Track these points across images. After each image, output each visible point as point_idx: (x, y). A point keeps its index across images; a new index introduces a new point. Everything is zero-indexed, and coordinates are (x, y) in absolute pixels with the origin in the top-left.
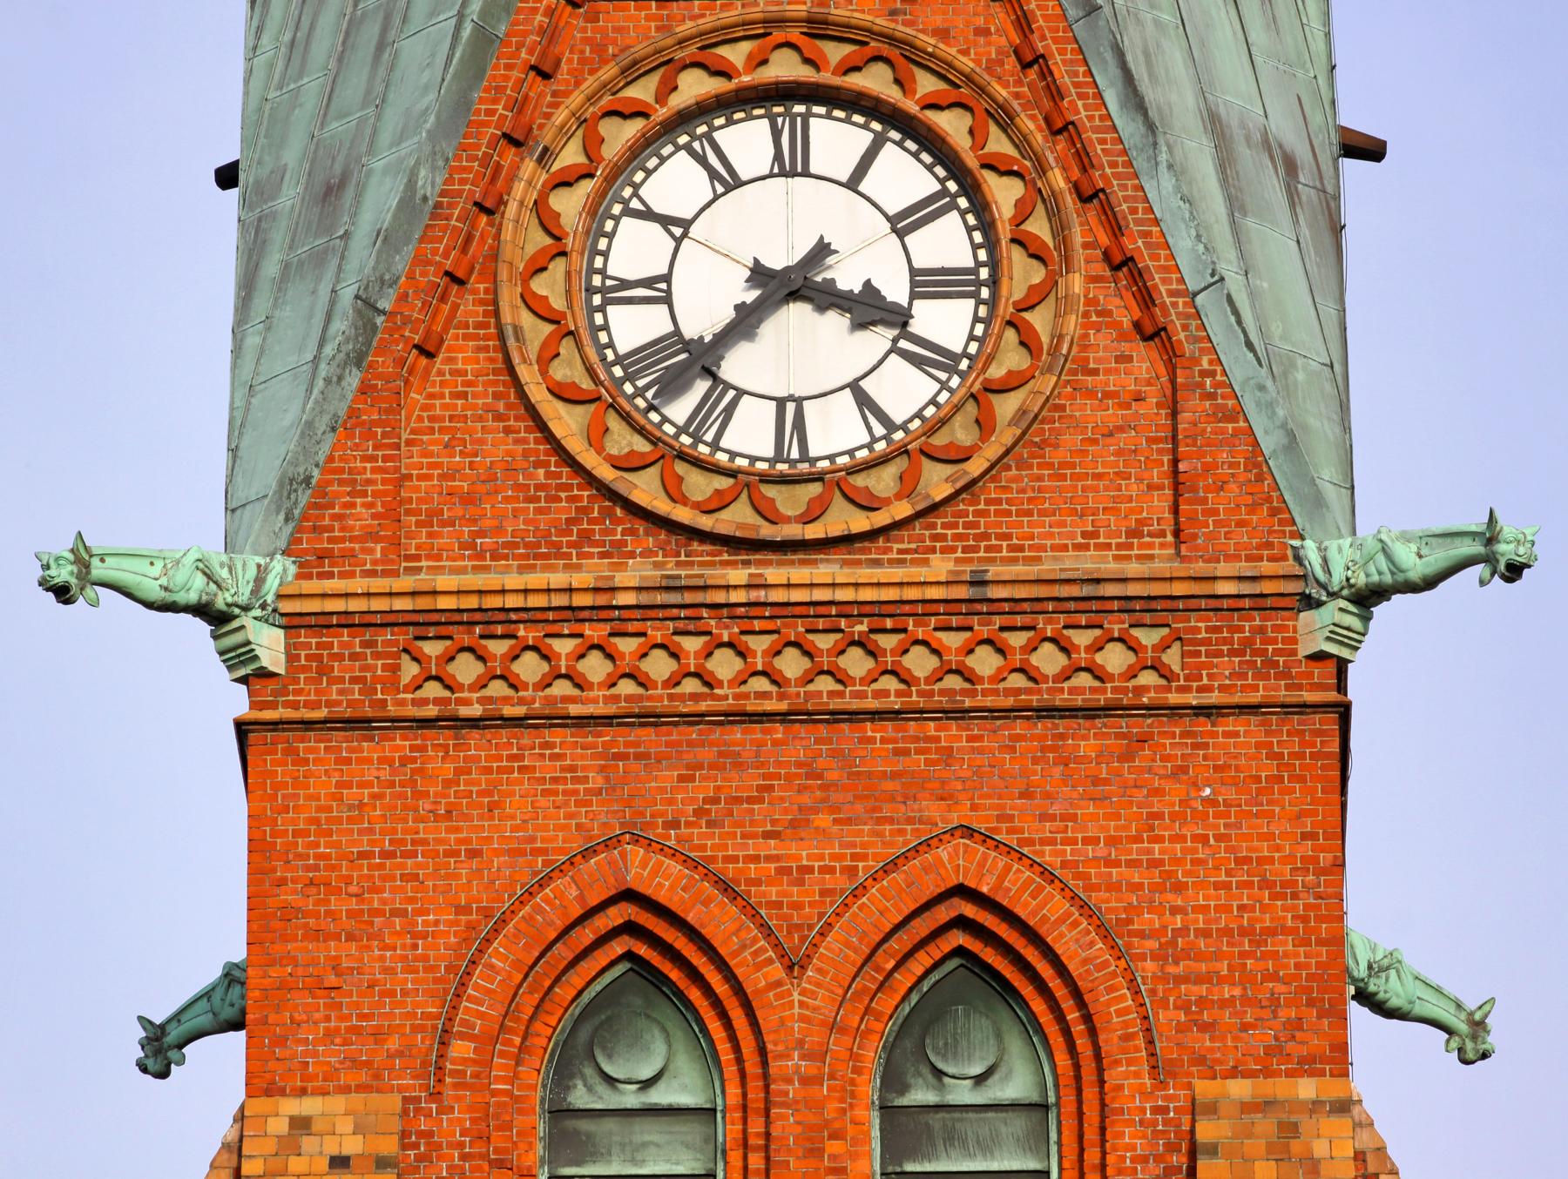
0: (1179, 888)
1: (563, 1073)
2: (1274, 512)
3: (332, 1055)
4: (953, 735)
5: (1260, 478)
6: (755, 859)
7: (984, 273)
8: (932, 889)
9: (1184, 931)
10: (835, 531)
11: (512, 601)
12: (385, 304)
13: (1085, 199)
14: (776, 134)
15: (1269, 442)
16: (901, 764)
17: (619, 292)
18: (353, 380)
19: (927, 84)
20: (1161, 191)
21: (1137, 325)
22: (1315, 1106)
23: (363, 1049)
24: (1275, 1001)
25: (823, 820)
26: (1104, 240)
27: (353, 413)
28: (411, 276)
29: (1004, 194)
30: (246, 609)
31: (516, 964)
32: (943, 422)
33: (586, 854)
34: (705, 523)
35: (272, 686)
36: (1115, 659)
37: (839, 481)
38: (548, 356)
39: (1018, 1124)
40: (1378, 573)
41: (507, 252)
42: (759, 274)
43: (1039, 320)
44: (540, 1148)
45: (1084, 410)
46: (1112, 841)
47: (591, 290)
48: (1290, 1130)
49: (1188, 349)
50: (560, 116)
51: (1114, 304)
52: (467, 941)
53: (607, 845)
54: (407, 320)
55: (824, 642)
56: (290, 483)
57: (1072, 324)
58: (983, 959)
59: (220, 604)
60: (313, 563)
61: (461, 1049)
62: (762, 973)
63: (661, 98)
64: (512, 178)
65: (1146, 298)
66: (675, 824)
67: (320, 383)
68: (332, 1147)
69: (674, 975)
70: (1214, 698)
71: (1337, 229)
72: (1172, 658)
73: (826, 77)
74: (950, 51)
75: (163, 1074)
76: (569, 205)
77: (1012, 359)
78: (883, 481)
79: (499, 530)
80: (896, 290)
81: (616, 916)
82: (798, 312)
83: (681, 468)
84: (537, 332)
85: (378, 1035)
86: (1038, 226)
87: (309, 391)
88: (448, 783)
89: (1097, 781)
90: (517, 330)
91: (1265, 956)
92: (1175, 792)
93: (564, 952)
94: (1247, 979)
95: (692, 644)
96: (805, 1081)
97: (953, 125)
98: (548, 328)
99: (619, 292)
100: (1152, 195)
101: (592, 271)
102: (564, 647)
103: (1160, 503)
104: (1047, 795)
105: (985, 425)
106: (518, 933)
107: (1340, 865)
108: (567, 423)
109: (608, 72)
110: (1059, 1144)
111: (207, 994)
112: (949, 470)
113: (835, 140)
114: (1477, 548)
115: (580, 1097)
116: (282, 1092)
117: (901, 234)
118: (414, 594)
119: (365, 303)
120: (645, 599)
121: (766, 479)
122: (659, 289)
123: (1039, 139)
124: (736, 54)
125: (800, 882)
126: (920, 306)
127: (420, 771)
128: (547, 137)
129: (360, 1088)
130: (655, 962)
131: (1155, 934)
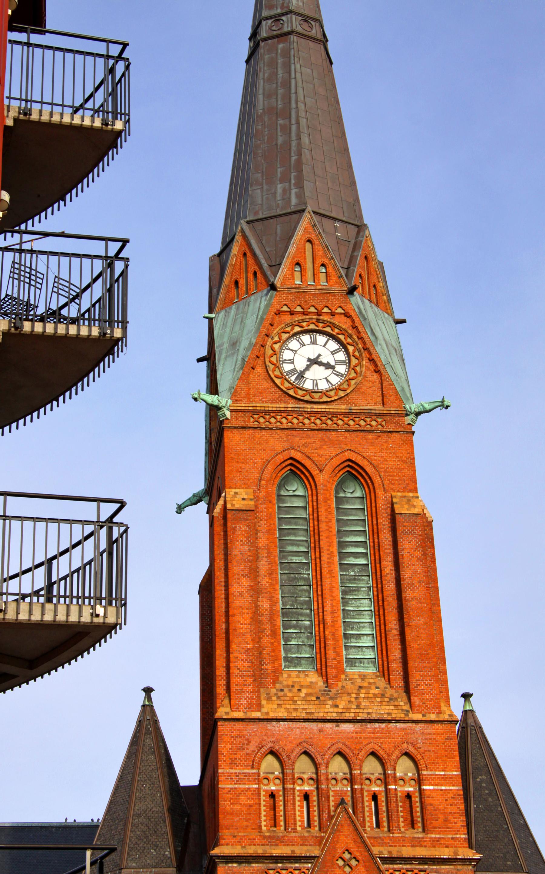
0: (387, 461)
1: (280, 488)
2: (400, 401)
3: (240, 482)
4: (347, 434)
5: (397, 395)
6: (313, 453)
7: (347, 361)
8: (344, 459)
9: (388, 468)
10: (325, 400)
11: (270, 409)
12: (246, 360)
13: (364, 349)
14: (311, 338)
15: (398, 389)
16: (338, 439)
17: (285, 361)
18: (241, 372)
19: (337, 330)
20: (378, 348)
21: (375, 370)
22: (413, 497)
23: (246, 482)
24: (404, 480)
25: (325, 447)
26: (368, 356)
27: (241, 377)
28: (250, 356)
29: (351, 349)
30: (224, 407)
31: (272, 469)
32: (342, 384)
33: (284, 451)
34: (302, 398)
35: (228, 421)
36: (374, 423)
37: (325, 393)
38: (273, 371)
39: (358, 501)
40: (421, 409)
41: (267, 353)
42: (309, 360)
43: (358, 369)
44: (276, 501)
45: (366, 383)
46: (375, 453)
47: (280, 361)
48: (409, 501)
49: (384, 374)
50: (275, 332)
51: (370, 367)
52: (263, 464)
53: (287, 449)
54: (250, 363)
55: (324, 418)
56: (231, 388)
57: (364, 369)
58: (353, 472)
59: (220, 406)
60: (235, 401)
61: (263, 482)
62: (315, 472)
63: (291, 330)
64: (267, 342)
65: (376, 365)
66: (299, 447)
67: (236, 372)
68: (242, 497)
69: (299, 473)
70: (391, 430)
71: (404, 361)
72: (384, 423)
73: (320, 328)
74: (340, 325)
75: (180, 513)
76: (276, 347)
77: (353, 375)
78: (332, 393)
79: (266, 398)
80: (333, 363)
81: (289, 462)
82: (316, 366)
83: (297, 389)
84: (272, 367)
85: (248, 479)
86: (357, 354)
87: (234, 373)
88: (259, 438)
89: (372, 443)
90: (269, 366)
91: (402, 473)
92: (385, 445)
93: (280, 467)
94: (399, 476)
95: (301, 418)
96: (324, 490)
97: (342, 337)
98: (273, 366)
99: (285, 361)
100: (377, 349)
101: (280, 358)
102: (279, 417)
103: (380, 399)
104: (364, 445)
105: (349, 385)
106: (272, 463)
107: (414, 458)
108: (278, 381)
109: (283, 325)
110: (367, 504)
111: (189, 499)
112: (343, 392)
113: (321, 339)
114: (440, 404)
115: (282, 493)
116: (232, 488)
117: (333, 354)
118: (253, 407)
119: (243, 360)
120: (293, 409)
121: (312, 392)
122: (292, 361)
123: (357, 339)
124: (304, 324)
125: (321, 457)
126: (336, 366)
127: (255, 436)
128: (273, 335)
129: (246, 488)
130: (296, 470)
131: (384, 468)
